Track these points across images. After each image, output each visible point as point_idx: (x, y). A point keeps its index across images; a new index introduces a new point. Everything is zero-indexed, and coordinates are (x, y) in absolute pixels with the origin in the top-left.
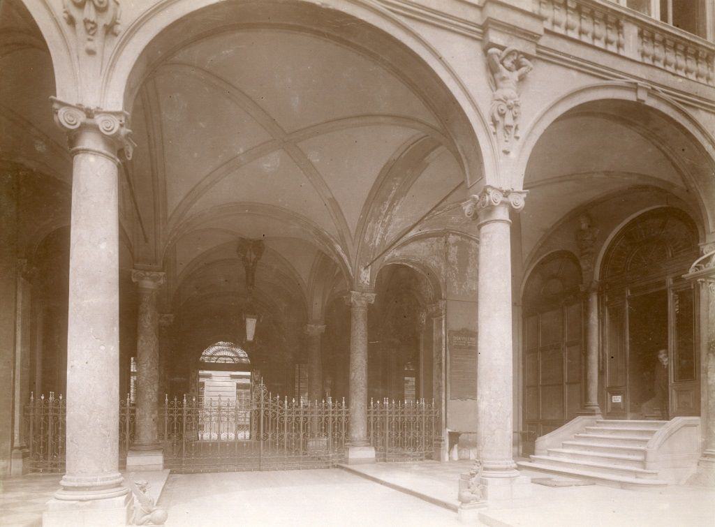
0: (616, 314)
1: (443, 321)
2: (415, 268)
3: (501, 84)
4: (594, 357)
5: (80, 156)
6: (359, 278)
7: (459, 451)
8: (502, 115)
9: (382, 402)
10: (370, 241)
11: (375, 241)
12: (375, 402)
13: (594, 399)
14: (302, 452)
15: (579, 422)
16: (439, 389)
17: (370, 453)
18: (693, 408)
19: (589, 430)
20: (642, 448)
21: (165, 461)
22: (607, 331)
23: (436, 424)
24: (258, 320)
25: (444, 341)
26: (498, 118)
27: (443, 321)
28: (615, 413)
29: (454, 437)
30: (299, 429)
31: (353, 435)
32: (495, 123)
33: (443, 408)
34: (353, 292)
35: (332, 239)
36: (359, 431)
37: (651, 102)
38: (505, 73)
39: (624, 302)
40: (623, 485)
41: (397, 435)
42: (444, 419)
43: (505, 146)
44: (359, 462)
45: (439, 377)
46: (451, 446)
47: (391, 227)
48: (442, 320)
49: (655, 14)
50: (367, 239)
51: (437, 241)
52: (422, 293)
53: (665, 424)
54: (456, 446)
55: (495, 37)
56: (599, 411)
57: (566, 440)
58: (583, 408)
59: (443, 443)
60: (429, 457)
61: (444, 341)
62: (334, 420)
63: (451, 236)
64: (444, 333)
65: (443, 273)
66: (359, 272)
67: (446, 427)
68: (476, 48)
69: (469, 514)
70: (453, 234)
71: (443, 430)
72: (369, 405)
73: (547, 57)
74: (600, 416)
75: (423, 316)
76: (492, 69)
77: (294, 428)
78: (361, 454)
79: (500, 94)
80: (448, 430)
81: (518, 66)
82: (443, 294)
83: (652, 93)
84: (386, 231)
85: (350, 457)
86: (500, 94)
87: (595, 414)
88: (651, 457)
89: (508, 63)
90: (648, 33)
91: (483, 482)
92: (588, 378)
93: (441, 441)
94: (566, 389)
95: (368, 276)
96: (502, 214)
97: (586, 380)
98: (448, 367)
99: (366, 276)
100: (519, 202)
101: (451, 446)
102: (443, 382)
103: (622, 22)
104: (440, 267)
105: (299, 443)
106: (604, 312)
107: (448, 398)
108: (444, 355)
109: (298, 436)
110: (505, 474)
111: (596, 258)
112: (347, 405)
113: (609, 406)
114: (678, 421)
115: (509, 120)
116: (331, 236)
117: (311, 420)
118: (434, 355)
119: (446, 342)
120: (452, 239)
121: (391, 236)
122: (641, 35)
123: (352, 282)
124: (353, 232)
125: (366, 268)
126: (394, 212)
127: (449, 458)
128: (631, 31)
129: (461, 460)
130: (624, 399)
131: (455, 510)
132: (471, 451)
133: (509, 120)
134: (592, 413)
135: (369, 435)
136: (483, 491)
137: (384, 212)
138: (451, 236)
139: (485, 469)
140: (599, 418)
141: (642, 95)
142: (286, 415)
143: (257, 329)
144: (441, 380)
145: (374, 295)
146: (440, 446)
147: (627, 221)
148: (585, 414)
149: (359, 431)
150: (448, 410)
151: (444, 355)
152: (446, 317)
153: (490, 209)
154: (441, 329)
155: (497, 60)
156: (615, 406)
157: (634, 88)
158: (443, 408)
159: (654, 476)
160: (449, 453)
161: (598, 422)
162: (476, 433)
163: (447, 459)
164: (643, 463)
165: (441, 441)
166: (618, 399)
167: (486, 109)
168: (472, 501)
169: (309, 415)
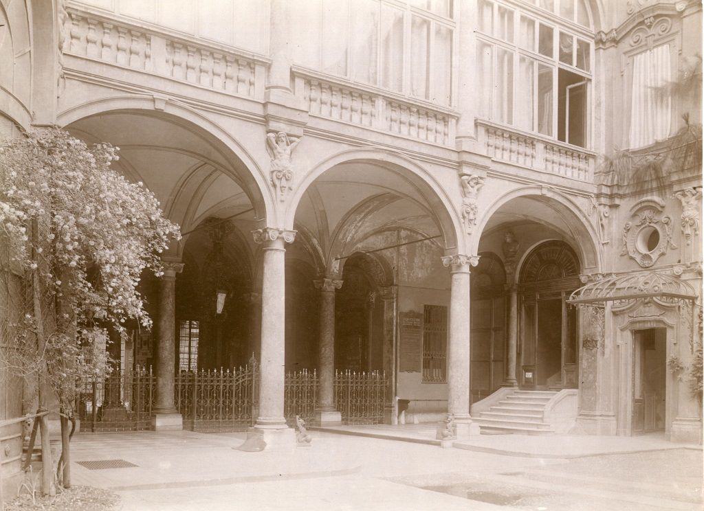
0: (530, 312)
1: (395, 304)
2: (371, 256)
3: (467, 195)
4: (513, 342)
5: (268, 252)
6: (331, 267)
7: (405, 416)
8: (468, 213)
9: (344, 373)
10: (343, 239)
11: (347, 238)
12: (339, 373)
13: (513, 374)
14: (234, 416)
15: (503, 392)
16: (390, 362)
17: (337, 417)
18: (573, 385)
19: (511, 398)
20: (541, 410)
21: (184, 423)
22: (523, 323)
23: (388, 393)
24: (227, 297)
25: (395, 321)
26: (466, 215)
27: (395, 304)
28: (528, 386)
29: (404, 405)
30: (232, 396)
31: (323, 402)
32: (464, 217)
33: (394, 379)
34: (326, 280)
35: (310, 234)
36: (328, 398)
37: (549, 195)
38: (471, 189)
39: (535, 304)
40: (529, 433)
41: (292, 402)
42: (394, 388)
43: (469, 231)
44: (328, 424)
45: (390, 352)
46: (400, 412)
47: (362, 228)
48: (393, 302)
49: (576, 21)
50: (341, 237)
51: (391, 235)
52: (372, 274)
53: (555, 394)
54: (403, 412)
55: (466, 170)
56: (517, 384)
57: (501, 400)
58: (506, 383)
59: (393, 409)
60: (381, 422)
61: (395, 321)
62: (185, 388)
63: (403, 231)
64: (395, 314)
65: (395, 262)
66: (331, 262)
67: (396, 395)
68: (454, 173)
69: (447, 443)
70: (405, 229)
71: (393, 398)
72: (335, 376)
73: (493, 175)
74: (517, 388)
75: (373, 296)
76: (463, 185)
77: (215, 395)
78: (331, 417)
79: (467, 201)
80: (398, 398)
81: (477, 183)
82: (395, 281)
83: (550, 190)
84: (356, 232)
85: (322, 420)
86: (467, 201)
87: (513, 386)
88: (546, 414)
89: (472, 183)
90: (549, 146)
91: (454, 426)
92: (509, 356)
93: (391, 407)
94: (493, 363)
95: (338, 266)
96: (466, 269)
97: (508, 359)
98: (398, 344)
99: (336, 266)
100: (476, 263)
101: (400, 412)
102: (394, 357)
103: (535, 143)
104: (393, 257)
105: (232, 409)
106: (521, 310)
107: (398, 370)
108: (394, 333)
109: (218, 402)
110: (466, 421)
111: (517, 265)
112: (318, 376)
113: (524, 380)
114: (565, 392)
115: (472, 216)
116: (310, 232)
117: (302, 389)
118: (385, 333)
119: (397, 323)
120: (403, 233)
121: (360, 234)
122: (546, 147)
123: (324, 271)
124: (330, 234)
125: (337, 259)
126: (366, 220)
127: (399, 422)
128: (540, 147)
129: (407, 423)
130: (533, 375)
131: (439, 444)
132: (415, 417)
133: (472, 216)
134: (511, 385)
135: (176, 403)
136: (454, 431)
137: (358, 219)
138: (403, 231)
139: (455, 419)
140: (516, 389)
141: (545, 192)
142: (180, 383)
143: (226, 302)
144: (392, 355)
145: (342, 281)
146: (391, 411)
147: (537, 244)
148: (506, 386)
149: (328, 398)
150: (398, 381)
151: (394, 333)
152: (397, 300)
153: (459, 266)
154: (393, 310)
155: (466, 182)
156: (527, 380)
157: (541, 188)
158: (394, 379)
159: (547, 427)
160: (398, 418)
161: (500, 403)
162: (447, 401)
163: (396, 423)
164: (542, 419)
165: (391, 407)
166: (529, 375)
167: (459, 208)
168: (449, 437)
169: (215, 383)
